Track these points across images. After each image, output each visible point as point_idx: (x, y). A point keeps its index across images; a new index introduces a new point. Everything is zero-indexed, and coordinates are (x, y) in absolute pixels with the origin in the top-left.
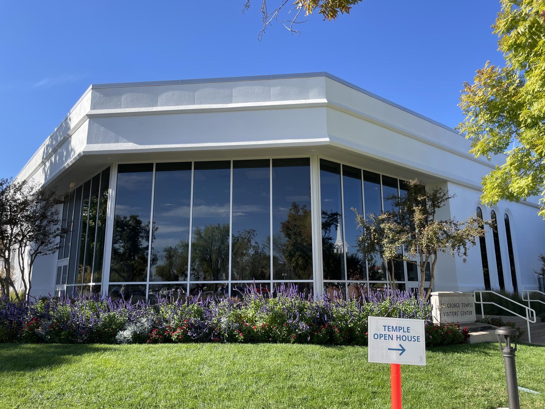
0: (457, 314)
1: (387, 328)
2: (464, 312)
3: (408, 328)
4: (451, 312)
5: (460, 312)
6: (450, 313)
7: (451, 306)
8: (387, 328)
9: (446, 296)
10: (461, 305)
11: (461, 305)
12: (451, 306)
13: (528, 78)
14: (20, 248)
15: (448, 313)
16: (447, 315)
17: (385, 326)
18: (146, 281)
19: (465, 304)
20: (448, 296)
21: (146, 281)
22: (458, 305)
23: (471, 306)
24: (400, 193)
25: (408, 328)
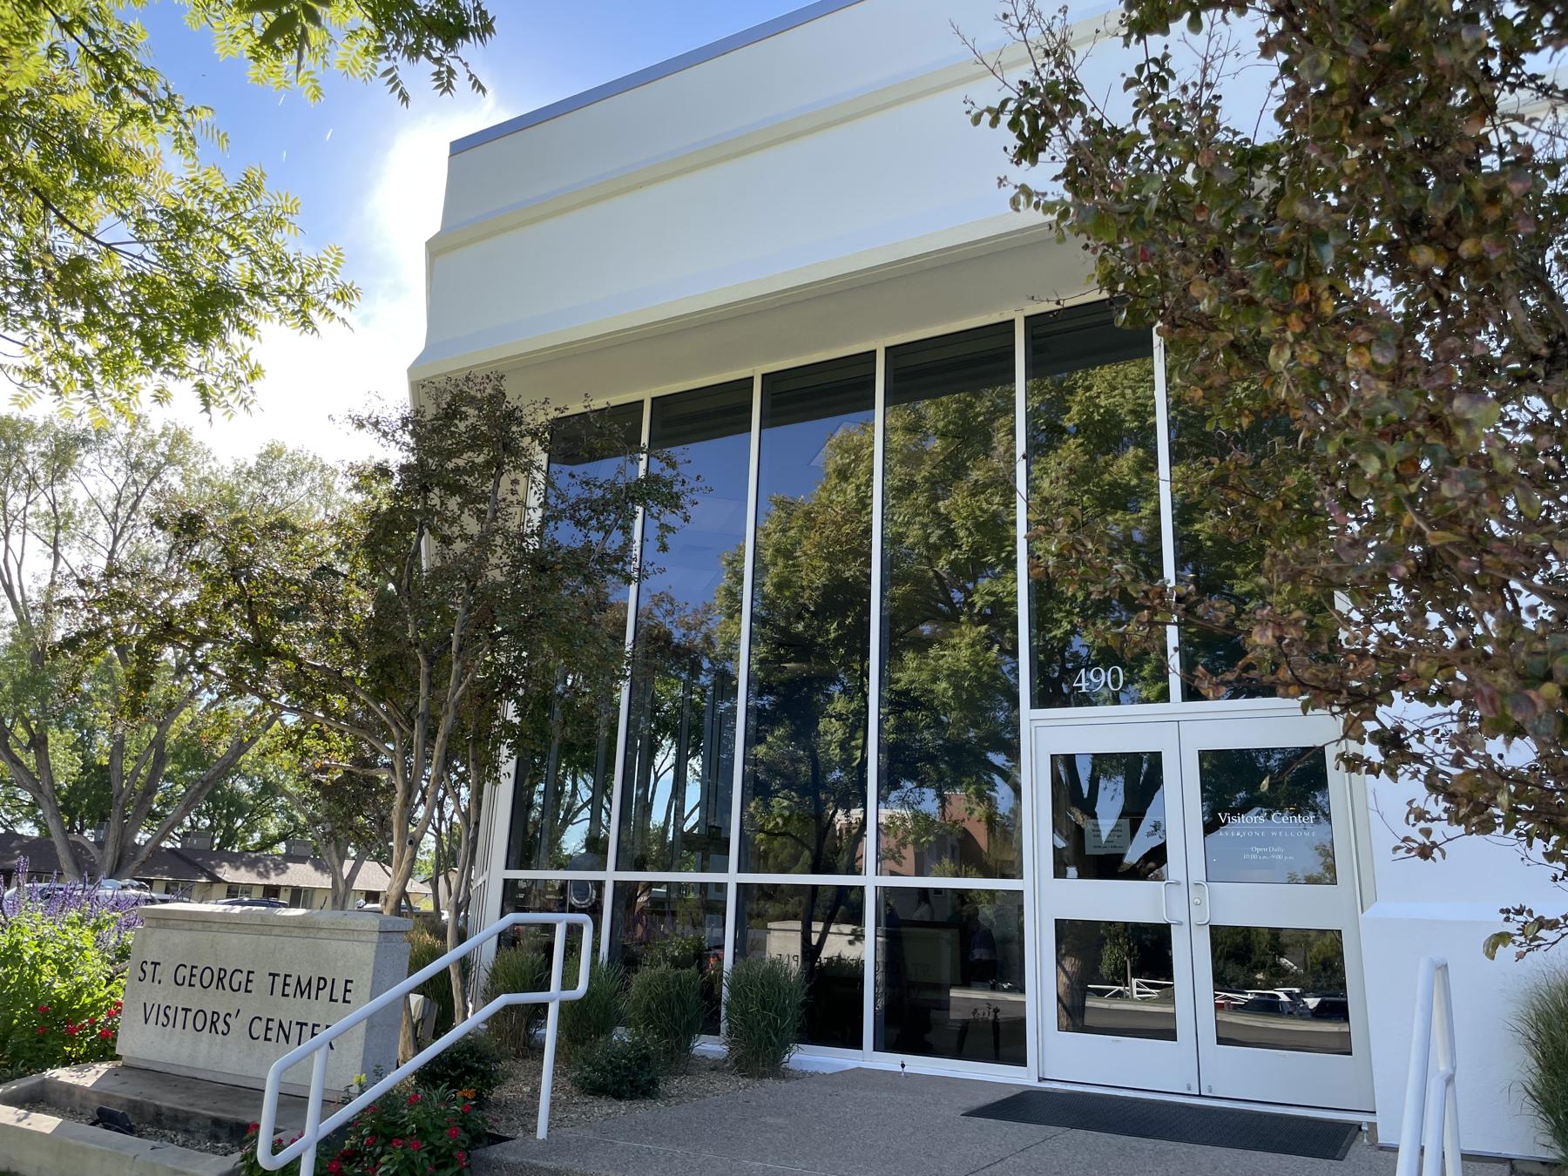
0: (221, 1026)
1: (279, 981)
2: (274, 1025)
3: (347, 981)
4: (186, 1010)
5: (245, 1018)
6: (181, 1014)
7: (195, 981)
8: (279, 981)
9: (187, 925)
10: (261, 981)
11: (261, 981)
12: (195, 981)
13: (1336, 709)
14: (442, 879)
15: (171, 1013)
16: (162, 1018)
17: (274, 975)
18: (862, 888)
19: (292, 981)
20: (200, 926)
21: (862, 888)
22: (242, 977)
23: (338, 994)
24: (61, 535)
25: (347, 981)
